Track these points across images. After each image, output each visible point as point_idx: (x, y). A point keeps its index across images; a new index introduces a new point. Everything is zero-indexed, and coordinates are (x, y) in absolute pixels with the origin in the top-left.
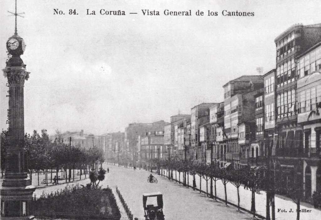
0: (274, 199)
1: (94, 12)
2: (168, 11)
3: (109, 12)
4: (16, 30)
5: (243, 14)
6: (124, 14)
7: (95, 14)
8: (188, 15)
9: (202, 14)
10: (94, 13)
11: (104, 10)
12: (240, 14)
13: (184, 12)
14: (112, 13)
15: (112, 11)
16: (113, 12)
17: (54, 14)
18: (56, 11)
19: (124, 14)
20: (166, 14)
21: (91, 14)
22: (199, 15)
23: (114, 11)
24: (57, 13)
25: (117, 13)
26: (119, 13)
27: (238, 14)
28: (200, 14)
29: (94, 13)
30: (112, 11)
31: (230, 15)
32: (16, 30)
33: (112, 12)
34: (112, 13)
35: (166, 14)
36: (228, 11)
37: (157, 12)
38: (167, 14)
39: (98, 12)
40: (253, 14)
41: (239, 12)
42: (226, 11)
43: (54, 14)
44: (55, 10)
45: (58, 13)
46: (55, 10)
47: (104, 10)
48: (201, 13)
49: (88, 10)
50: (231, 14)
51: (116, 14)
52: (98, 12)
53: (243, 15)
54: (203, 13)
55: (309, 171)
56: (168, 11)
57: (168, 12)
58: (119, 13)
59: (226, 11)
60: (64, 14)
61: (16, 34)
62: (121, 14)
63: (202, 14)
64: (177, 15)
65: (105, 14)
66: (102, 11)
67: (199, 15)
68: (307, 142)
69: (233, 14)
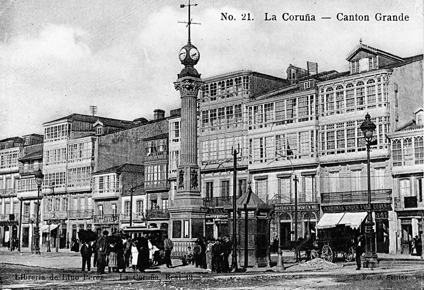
0: (132, 255)
1: (275, 16)
2: (380, 14)
3: (295, 17)
4: (189, 40)
5: (364, 17)
6: (314, 19)
7: (315, 20)
8: (348, 20)
9: (407, 19)
10: (275, 18)
11: (288, 14)
12: (361, 18)
13: (386, 16)
14: (298, 18)
15: (298, 16)
16: (299, 17)
17: (222, 19)
18: (224, 16)
19: (314, 19)
20: (378, 18)
21: (270, 20)
22: (397, 20)
23: (300, 16)
24: (226, 18)
25: (305, 19)
26: (308, 17)
27: (358, 18)
28: (404, 19)
29: (275, 18)
30: (298, 16)
31: (347, 20)
32: (189, 40)
33: (297, 17)
34: (298, 18)
35: (378, 18)
36: (344, 15)
37: (312, 16)
38: (380, 18)
39: (279, 17)
40: (407, 17)
41: (358, 15)
42: (342, 14)
43: (222, 19)
44: (223, 14)
45: (227, 18)
46: (223, 14)
47: (288, 14)
48: (405, 18)
49: (266, 14)
50: (349, 18)
51: (303, 20)
52: (279, 17)
53: (364, 19)
54: (408, 17)
55: (206, 236)
56: (380, 14)
57: (381, 16)
58: (308, 17)
59: (342, 14)
60: (235, 20)
61: (189, 42)
62: (310, 19)
63: (407, 19)
64: (402, 20)
65: (289, 19)
66: (285, 15)
67: (402, 20)
68: (228, 193)
69: (352, 19)
